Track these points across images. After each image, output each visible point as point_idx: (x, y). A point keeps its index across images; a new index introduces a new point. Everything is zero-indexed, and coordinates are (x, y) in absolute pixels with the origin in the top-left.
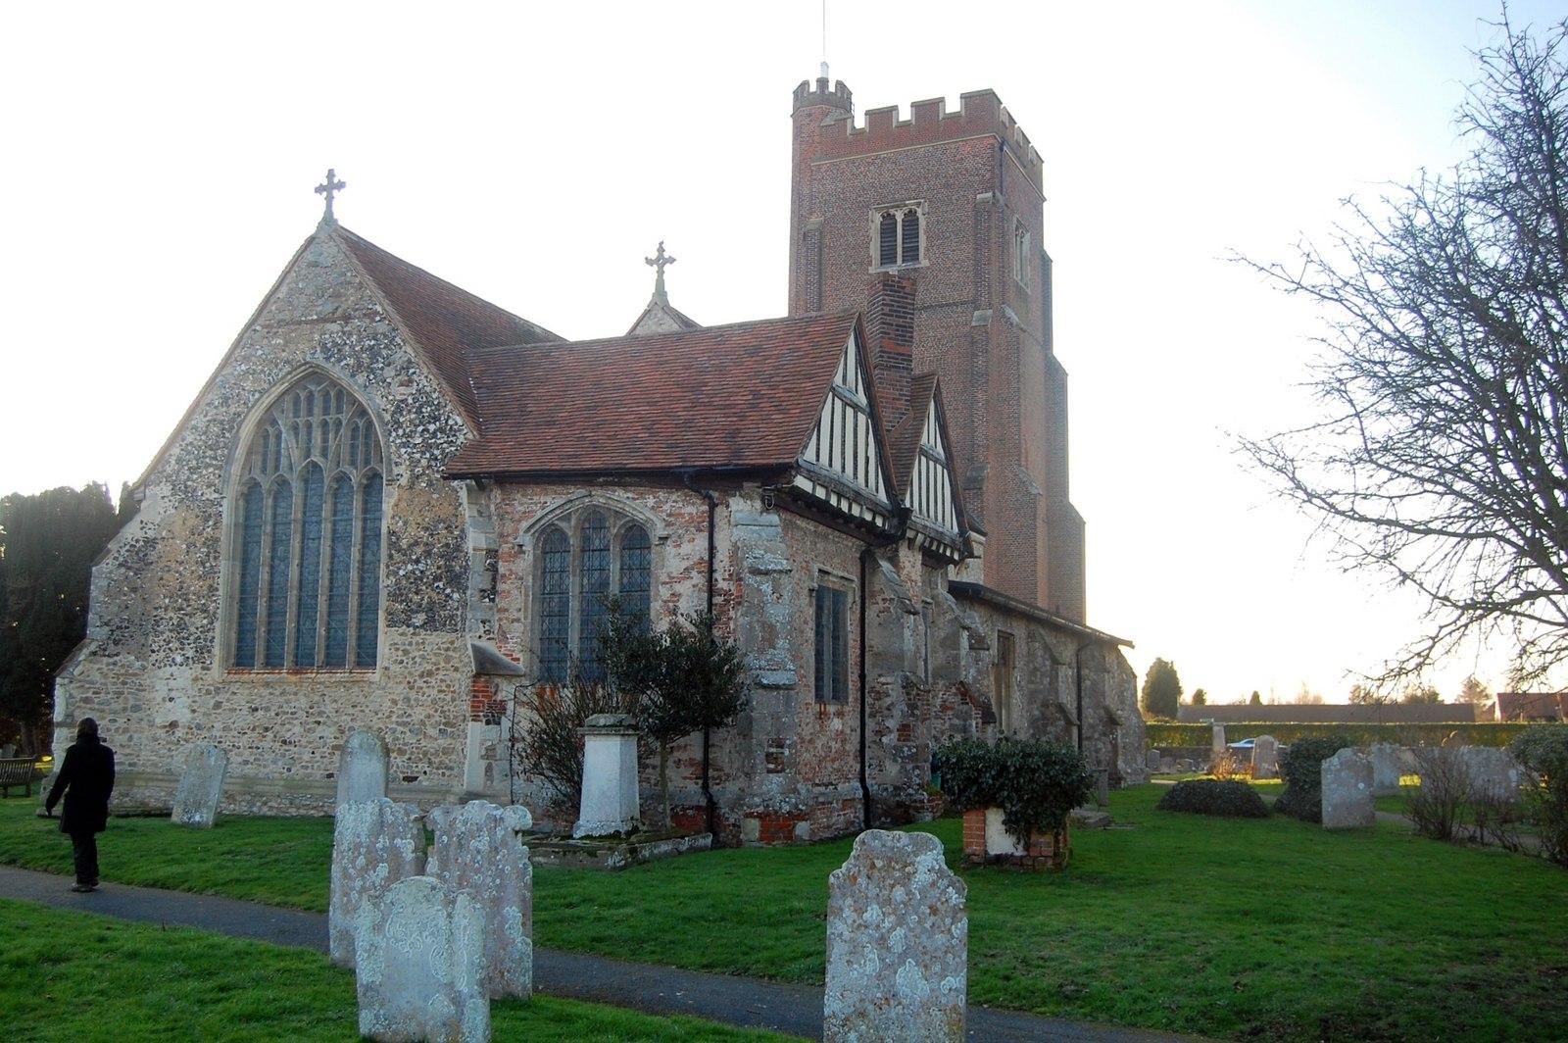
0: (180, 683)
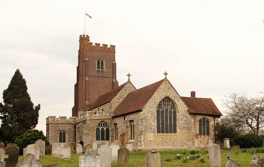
0: (151, 135)
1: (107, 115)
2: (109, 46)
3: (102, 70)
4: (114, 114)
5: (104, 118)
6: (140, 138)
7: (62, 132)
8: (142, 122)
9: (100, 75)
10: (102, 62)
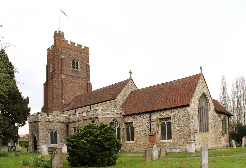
1: (119, 112)
2: (83, 47)
3: (77, 70)
4: (124, 112)
5: (115, 116)
6: (194, 137)
7: (54, 132)
8: (193, 119)
9: (76, 75)
10: (77, 62)
